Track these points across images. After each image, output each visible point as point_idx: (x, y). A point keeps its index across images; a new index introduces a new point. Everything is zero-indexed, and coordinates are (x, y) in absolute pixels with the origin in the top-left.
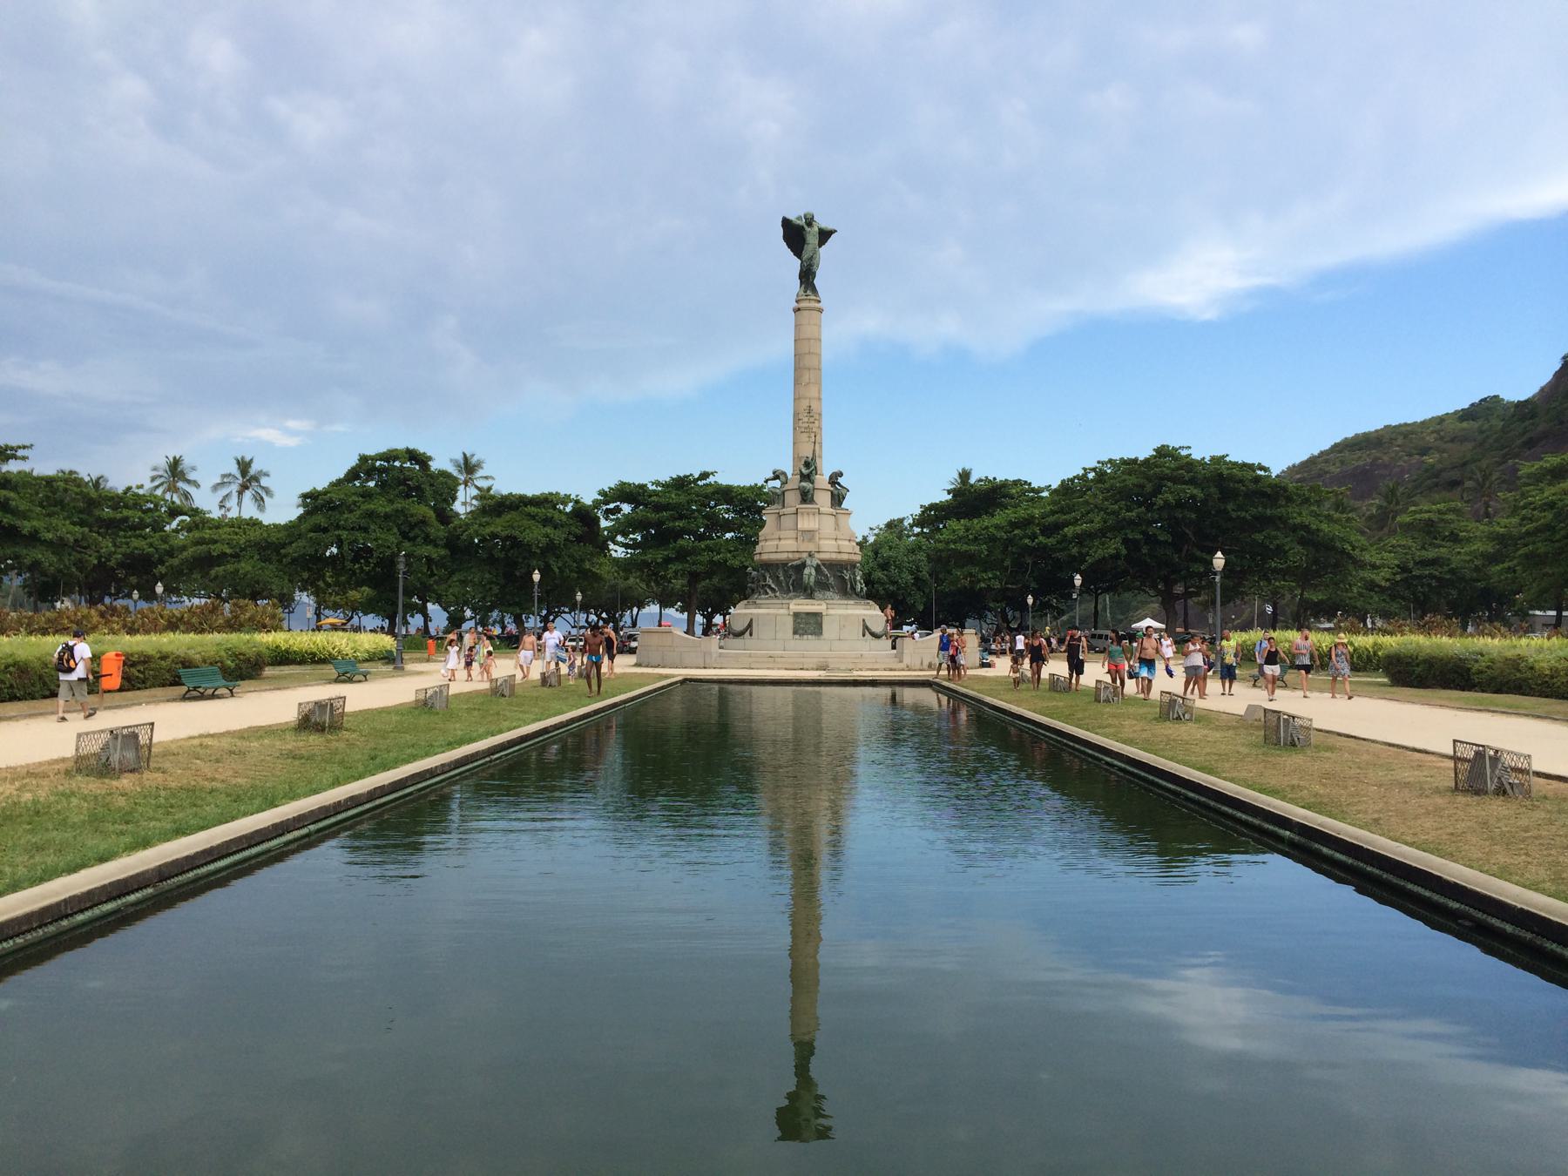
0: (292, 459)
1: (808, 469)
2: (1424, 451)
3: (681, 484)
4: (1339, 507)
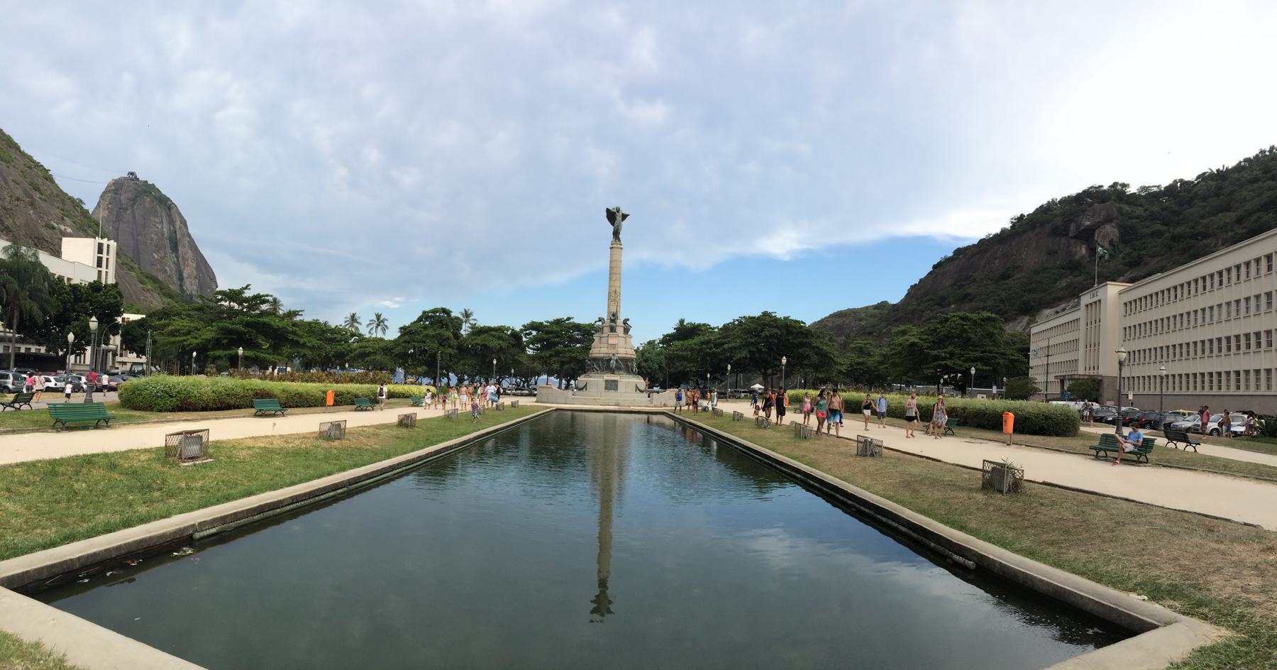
0: (391, 312)
1: (614, 317)
2: (861, 320)
3: (558, 322)
4: (831, 340)
